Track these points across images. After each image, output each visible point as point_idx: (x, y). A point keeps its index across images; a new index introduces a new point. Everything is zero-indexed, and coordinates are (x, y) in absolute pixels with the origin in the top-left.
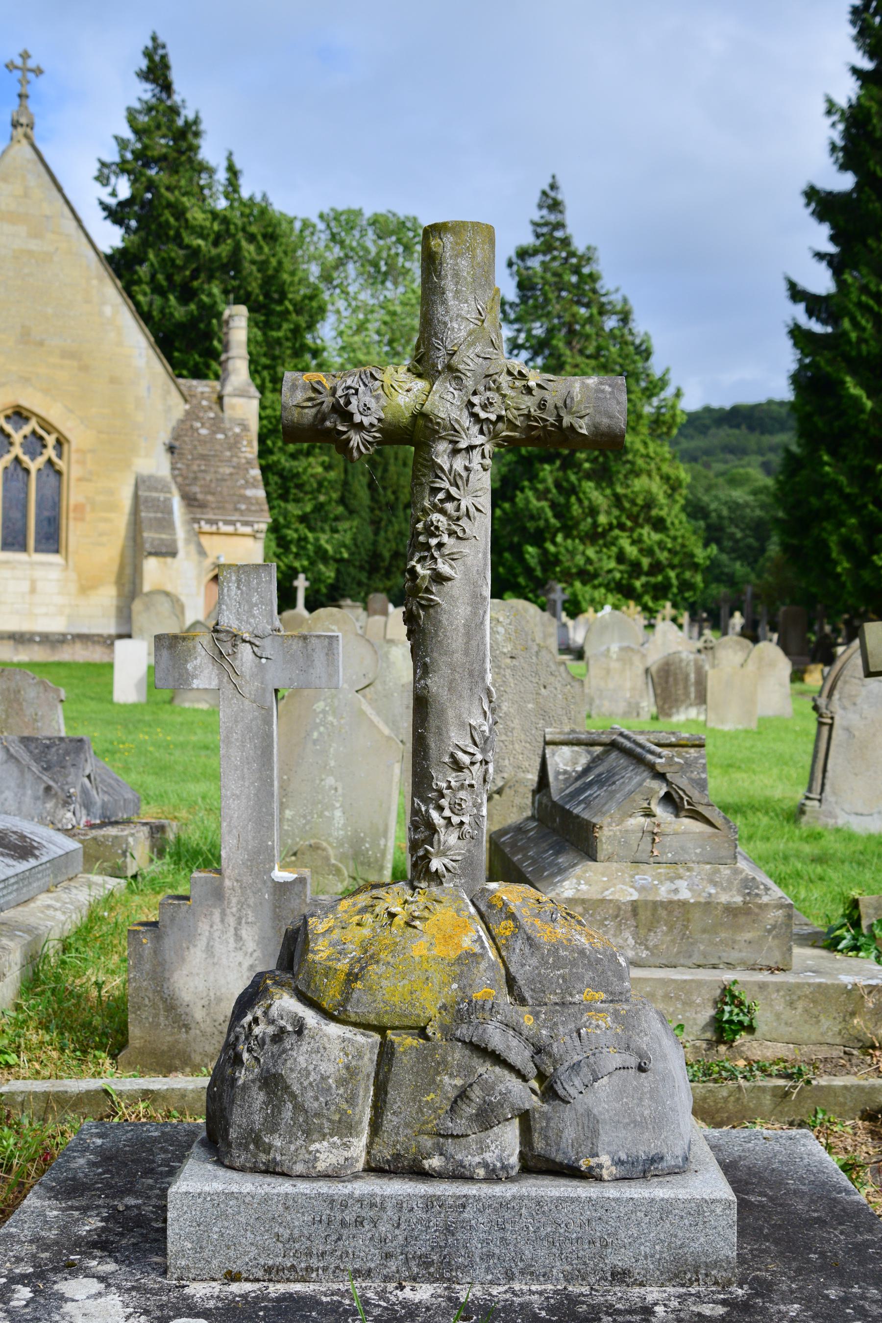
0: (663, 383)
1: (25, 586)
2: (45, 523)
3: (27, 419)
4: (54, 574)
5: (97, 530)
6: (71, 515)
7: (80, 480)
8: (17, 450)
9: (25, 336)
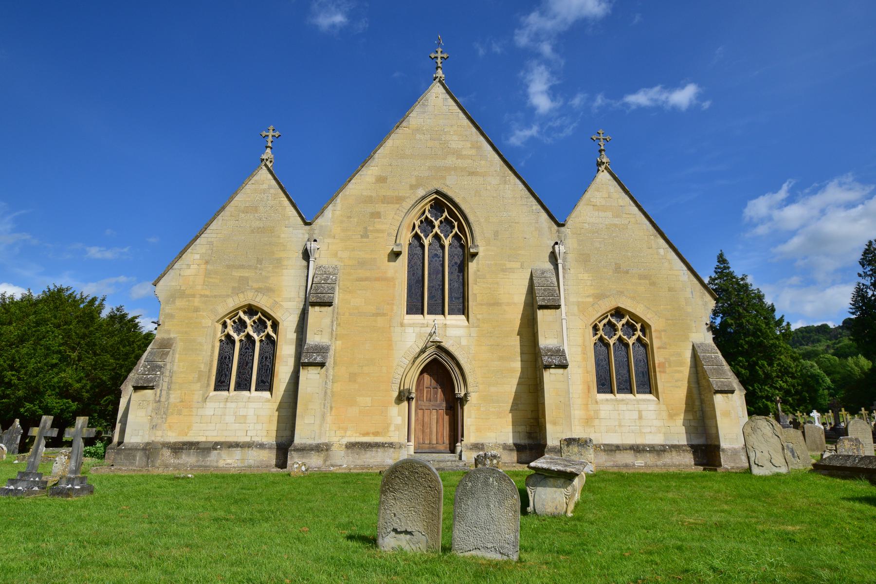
0: (781, 320)
1: (635, 415)
2: (641, 375)
3: (622, 317)
4: (652, 407)
5: (674, 381)
6: (657, 369)
7: (659, 348)
8: (620, 333)
9: (618, 269)
